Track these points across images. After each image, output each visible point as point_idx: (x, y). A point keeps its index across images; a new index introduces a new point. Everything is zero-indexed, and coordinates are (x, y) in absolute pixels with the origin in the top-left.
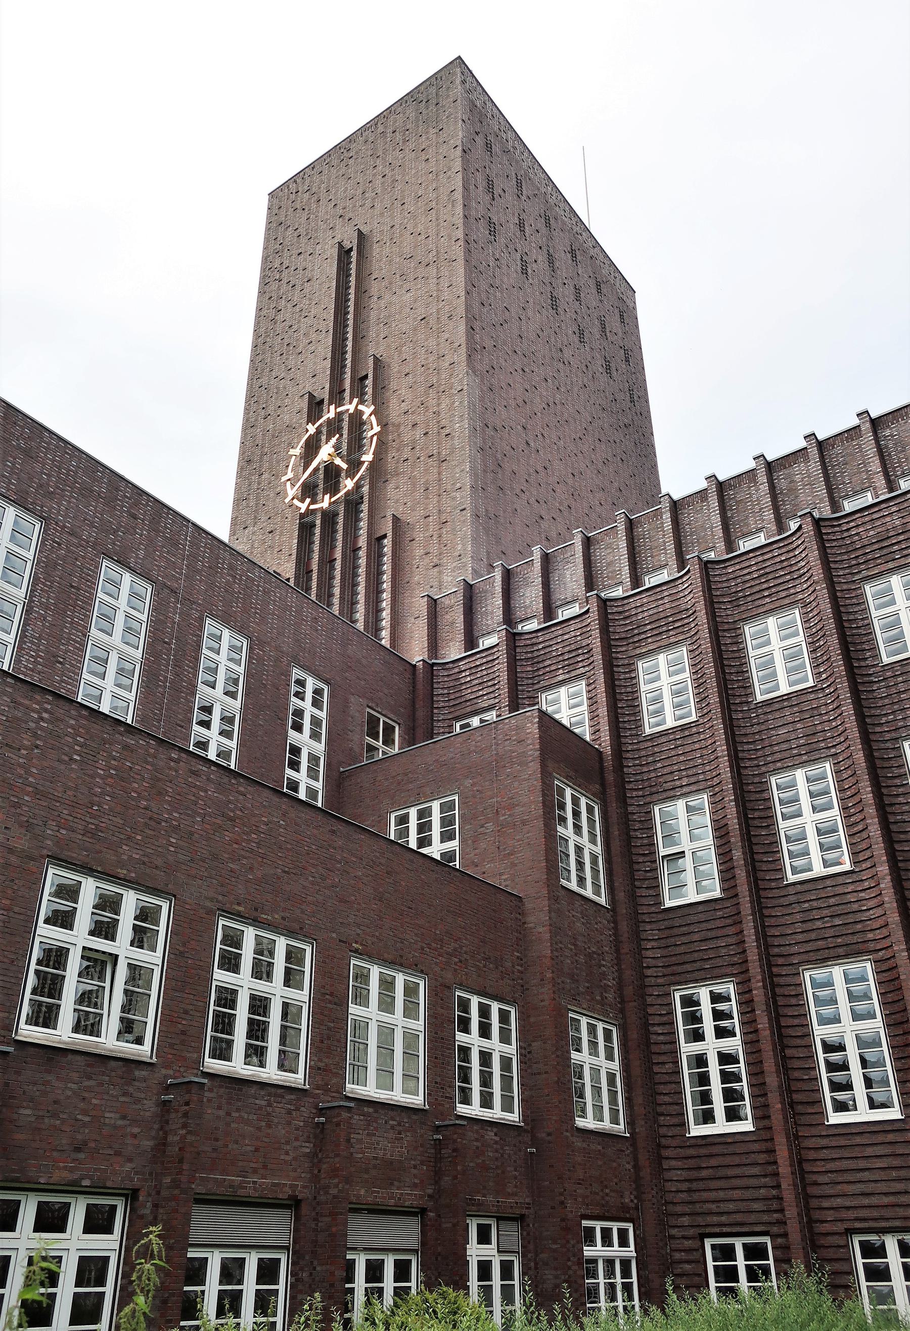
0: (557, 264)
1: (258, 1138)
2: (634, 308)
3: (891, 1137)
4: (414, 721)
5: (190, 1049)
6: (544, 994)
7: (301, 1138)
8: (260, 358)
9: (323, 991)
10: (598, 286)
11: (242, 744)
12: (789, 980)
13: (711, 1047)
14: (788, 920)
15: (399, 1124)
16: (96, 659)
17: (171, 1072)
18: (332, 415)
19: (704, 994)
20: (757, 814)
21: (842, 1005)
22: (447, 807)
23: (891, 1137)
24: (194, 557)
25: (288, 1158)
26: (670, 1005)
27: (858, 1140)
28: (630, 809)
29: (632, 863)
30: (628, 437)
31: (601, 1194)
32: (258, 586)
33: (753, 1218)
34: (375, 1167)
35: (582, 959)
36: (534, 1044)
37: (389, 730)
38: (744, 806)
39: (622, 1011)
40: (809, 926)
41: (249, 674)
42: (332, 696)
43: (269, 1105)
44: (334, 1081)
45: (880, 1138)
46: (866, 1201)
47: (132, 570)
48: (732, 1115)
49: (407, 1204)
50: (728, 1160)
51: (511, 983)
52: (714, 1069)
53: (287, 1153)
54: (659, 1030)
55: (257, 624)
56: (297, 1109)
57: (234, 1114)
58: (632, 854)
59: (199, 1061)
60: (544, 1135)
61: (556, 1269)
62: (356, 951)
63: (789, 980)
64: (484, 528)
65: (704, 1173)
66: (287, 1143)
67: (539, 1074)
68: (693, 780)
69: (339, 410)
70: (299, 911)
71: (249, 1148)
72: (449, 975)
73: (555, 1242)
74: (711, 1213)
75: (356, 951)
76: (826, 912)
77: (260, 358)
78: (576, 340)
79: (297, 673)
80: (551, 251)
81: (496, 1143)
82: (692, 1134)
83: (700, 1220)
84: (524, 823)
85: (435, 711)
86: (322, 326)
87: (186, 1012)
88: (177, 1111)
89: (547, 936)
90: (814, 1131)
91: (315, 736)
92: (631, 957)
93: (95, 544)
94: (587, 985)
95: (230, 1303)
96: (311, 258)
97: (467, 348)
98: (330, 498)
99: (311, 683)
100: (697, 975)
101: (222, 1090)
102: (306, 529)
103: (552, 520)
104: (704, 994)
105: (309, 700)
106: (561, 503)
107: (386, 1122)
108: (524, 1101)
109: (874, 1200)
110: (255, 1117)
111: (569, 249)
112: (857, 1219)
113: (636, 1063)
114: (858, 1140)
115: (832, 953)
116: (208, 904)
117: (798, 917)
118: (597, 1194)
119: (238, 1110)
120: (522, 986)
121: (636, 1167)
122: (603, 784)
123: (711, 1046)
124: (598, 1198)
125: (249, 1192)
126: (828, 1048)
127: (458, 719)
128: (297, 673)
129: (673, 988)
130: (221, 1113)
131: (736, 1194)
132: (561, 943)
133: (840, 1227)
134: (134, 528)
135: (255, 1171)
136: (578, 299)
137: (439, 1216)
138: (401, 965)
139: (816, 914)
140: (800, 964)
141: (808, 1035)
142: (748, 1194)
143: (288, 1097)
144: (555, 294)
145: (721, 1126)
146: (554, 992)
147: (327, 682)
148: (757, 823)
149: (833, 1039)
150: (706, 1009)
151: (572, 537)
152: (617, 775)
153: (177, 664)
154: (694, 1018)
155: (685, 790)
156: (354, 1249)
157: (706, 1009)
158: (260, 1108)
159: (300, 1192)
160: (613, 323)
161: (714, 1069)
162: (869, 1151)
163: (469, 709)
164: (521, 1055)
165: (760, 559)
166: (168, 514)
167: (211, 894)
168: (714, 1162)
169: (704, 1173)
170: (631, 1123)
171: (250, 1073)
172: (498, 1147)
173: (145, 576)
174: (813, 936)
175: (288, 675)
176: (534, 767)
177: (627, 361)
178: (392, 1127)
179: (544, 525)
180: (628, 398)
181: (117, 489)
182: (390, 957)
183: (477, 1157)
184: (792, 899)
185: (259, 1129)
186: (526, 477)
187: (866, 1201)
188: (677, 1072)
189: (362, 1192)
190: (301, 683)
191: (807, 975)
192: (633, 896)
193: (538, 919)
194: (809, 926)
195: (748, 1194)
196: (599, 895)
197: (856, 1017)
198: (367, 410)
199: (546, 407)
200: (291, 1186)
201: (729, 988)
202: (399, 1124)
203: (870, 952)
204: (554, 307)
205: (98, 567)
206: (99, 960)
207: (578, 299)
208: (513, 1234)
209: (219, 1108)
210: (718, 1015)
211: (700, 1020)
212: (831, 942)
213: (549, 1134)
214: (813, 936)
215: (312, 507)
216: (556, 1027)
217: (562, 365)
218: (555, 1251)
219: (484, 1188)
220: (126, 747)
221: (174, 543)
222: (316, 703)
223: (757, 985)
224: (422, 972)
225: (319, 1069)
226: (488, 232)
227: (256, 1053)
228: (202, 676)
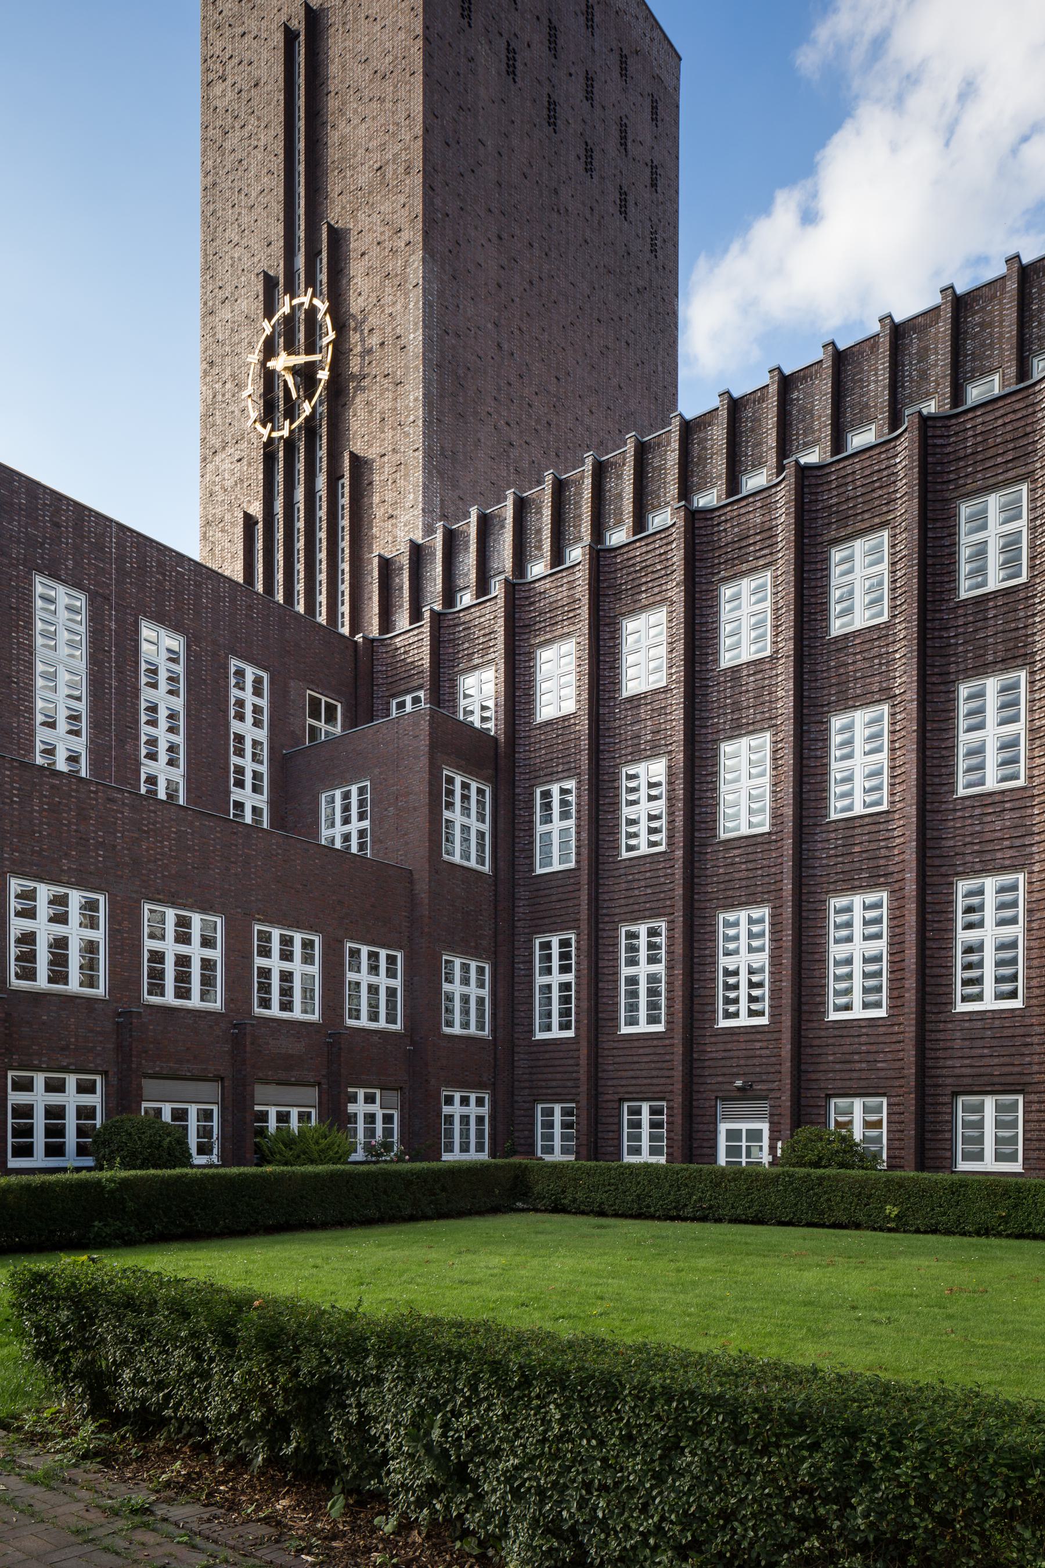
0: (561, 42)
2: (677, 89)
3: (655, 1042)
4: (356, 698)
8: (211, 207)
10: (623, 60)
11: (189, 738)
12: (611, 933)
14: (616, 888)
16: (45, 676)
18: (286, 309)
20: (607, 800)
21: (988, 917)
22: (362, 791)
23: (655, 1042)
24: (121, 559)
26: (531, 949)
27: (636, 1044)
28: (518, 791)
29: (514, 837)
30: (640, 307)
32: (189, 580)
33: (566, 1091)
35: (459, 916)
37: (331, 709)
38: (597, 793)
39: (495, 953)
40: (630, 893)
41: (189, 672)
42: (272, 682)
45: (649, 1043)
46: (634, 1082)
47: (65, 582)
50: (556, 1055)
52: (555, 994)
54: (521, 966)
55: (191, 620)
58: (512, 831)
63: (611, 933)
64: (438, 472)
65: (541, 1063)
68: (566, 767)
69: (295, 302)
74: (541, 1088)
76: (643, 883)
77: (211, 207)
78: (581, 168)
79: (234, 663)
80: (554, 18)
84: (415, 809)
86: (273, 167)
89: (426, 901)
90: (610, 1038)
91: (257, 723)
92: (503, 910)
93: (25, 560)
96: (255, 44)
97: (424, 222)
98: (291, 423)
99: (250, 672)
100: (551, 927)
102: (269, 459)
103: (525, 446)
105: (248, 688)
106: (538, 421)
108: (406, 1016)
109: (639, 1081)
111: (584, 7)
114: (636, 1044)
115: (641, 914)
117: (624, 886)
121: (495, 1059)
122: (496, 770)
126: (728, 973)
128: (234, 663)
131: (559, 1076)
133: (617, 1097)
134: (59, 538)
136: (589, 96)
139: (635, 885)
140: (620, 921)
141: (715, 963)
142: (566, 1076)
144: (554, 97)
145: (556, 1033)
147: (265, 668)
148: (605, 808)
149: (731, 968)
150: (643, 942)
151: (505, 499)
152: (507, 760)
153: (120, 670)
154: (633, 949)
155: (561, 776)
157: (643, 942)
160: (641, 127)
161: (555, 994)
162: (641, 1051)
163: (402, 687)
165: (644, 549)
166: (89, 516)
168: (547, 1056)
169: (541, 1063)
170: (494, 1030)
173: (78, 585)
174: (631, 901)
175: (226, 667)
176: (424, 761)
177: (654, 185)
179: (514, 453)
180: (648, 247)
181: (36, 498)
184: (622, 871)
186: (494, 393)
187: (634, 1082)
188: (531, 996)
190: (240, 673)
191: (721, 916)
192: (512, 865)
193: (422, 887)
194: (630, 893)
195: (566, 1076)
196: (483, 864)
197: (751, 950)
198: (322, 306)
199: (527, 287)
201: (662, 925)
203: (665, 915)
204: (552, 120)
205: (31, 584)
206: (60, 929)
207: (589, 96)
208: (394, 1097)
210: (651, 946)
211: (637, 950)
212: (642, 907)
214: (631, 901)
215: (275, 435)
217: (555, 215)
220: (53, 787)
221: (99, 547)
222: (257, 692)
223: (788, 912)
226: (458, 14)
228: (144, 680)
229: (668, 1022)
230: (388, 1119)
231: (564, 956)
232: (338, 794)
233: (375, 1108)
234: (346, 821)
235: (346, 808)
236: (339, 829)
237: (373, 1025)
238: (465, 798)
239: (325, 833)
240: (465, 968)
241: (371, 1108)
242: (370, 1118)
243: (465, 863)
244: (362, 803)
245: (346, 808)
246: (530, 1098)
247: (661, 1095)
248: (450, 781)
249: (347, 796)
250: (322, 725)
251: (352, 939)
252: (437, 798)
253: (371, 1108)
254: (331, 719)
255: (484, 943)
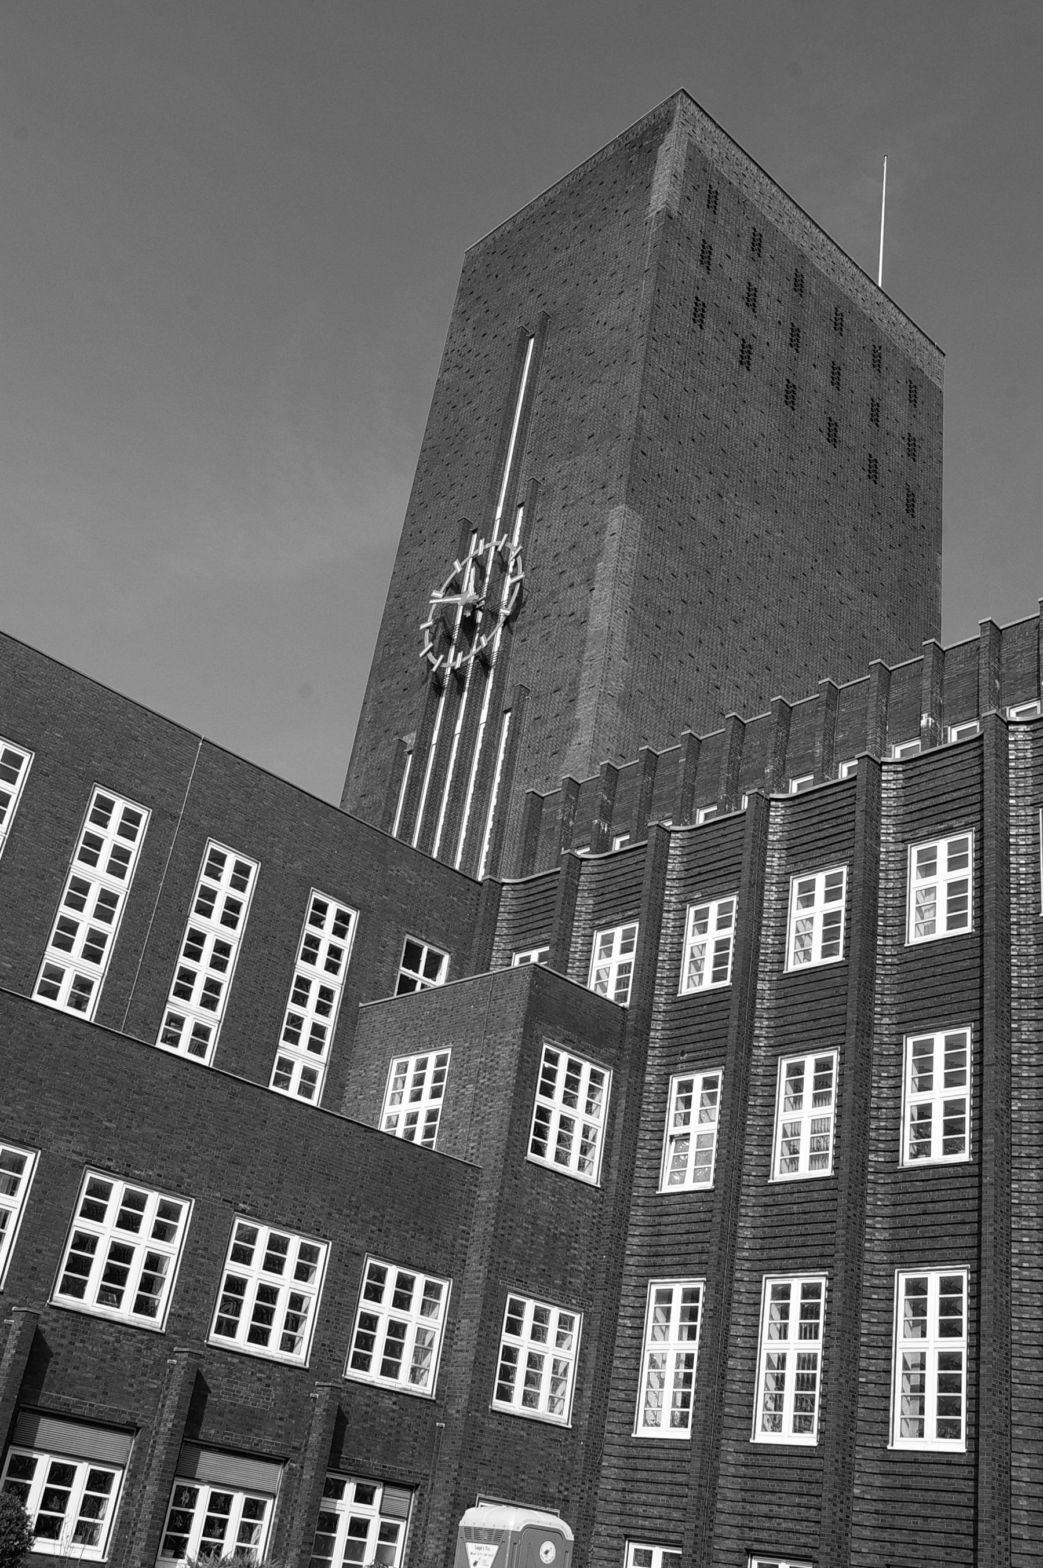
1: (100, 1368)
5: (39, 1284)
6: (476, 1270)
7: (149, 1375)
9: (195, 1245)
13: (672, 1347)
15: (269, 1377)
17: (17, 1301)
19: (933, 1279)
25: (130, 1390)
31: (514, 1478)
34: (231, 1412)
36: (463, 1321)
43: (118, 1341)
44: (195, 1329)
48: (947, 1430)
49: (264, 1451)
51: (449, 1257)
52: (791, 1372)
53: (131, 1385)
54: (741, 1320)
56: (149, 1348)
57: (77, 1344)
59: (49, 1294)
60: (454, 1412)
61: (439, 1539)
62: (243, 1211)
66: (133, 1376)
67: (461, 1351)
70: (179, 1169)
71: (89, 1375)
72: (362, 1243)
73: (442, 1515)
75: (243, 1211)
81: (393, 1411)
82: (757, 1441)
83: (627, 1520)
85: (496, 939)
87: (39, 1251)
88: (13, 1333)
94: (542, 1267)
95: (354, 1551)
101: (67, 1323)
104: (933, 1279)
107: (252, 1374)
110: (100, 1350)
112: (756, 1540)
113: (592, 1351)
116: (75, 1157)
118: (509, 1478)
119: (82, 1341)
120: (464, 1261)
123: (934, 1345)
124: (507, 1481)
125: (84, 1411)
127: (517, 950)
129: (651, 1281)
130: (65, 1342)
132: (512, 1220)
135: (94, 1395)
137: (302, 1467)
138: (298, 1228)
143: (140, 1337)
146: (489, 1271)
156: (199, 1480)
158: (107, 1343)
159: (140, 1421)
164: (447, 1330)
167: (79, 1148)
168: (651, 1464)
171: (100, 1311)
172: (396, 1415)
178: (260, 1380)
182: (285, 1220)
183: (365, 1421)
185: (103, 1360)
189: (213, 1432)
200: (131, 1414)
202: (269, 1377)
209: (63, 1337)
213: (458, 1412)
216: (484, 1307)
218: (441, 1522)
219: (369, 1451)
224: (325, 1237)
225: (180, 1316)
227: (110, 1295)
229: (820, 1432)
230: (388, 1533)
231: (948, 1307)
232: (412, 1061)
233: (370, 1512)
234: (416, 1097)
235: (419, 1081)
236: (407, 1106)
237: (387, 1383)
238: (572, 1083)
239: (388, 1110)
240: (540, 1316)
241: (362, 1511)
242: (359, 1527)
243: (560, 1168)
244: (438, 1077)
245: (419, 1081)
246: (620, 1531)
247: (804, 1551)
248: (553, 1058)
249: (422, 1065)
250: (419, 976)
251: (376, 1254)
252: (529, 1078)
253: (362, 1511)
254: (431, 972)
255: (577, 1282)
